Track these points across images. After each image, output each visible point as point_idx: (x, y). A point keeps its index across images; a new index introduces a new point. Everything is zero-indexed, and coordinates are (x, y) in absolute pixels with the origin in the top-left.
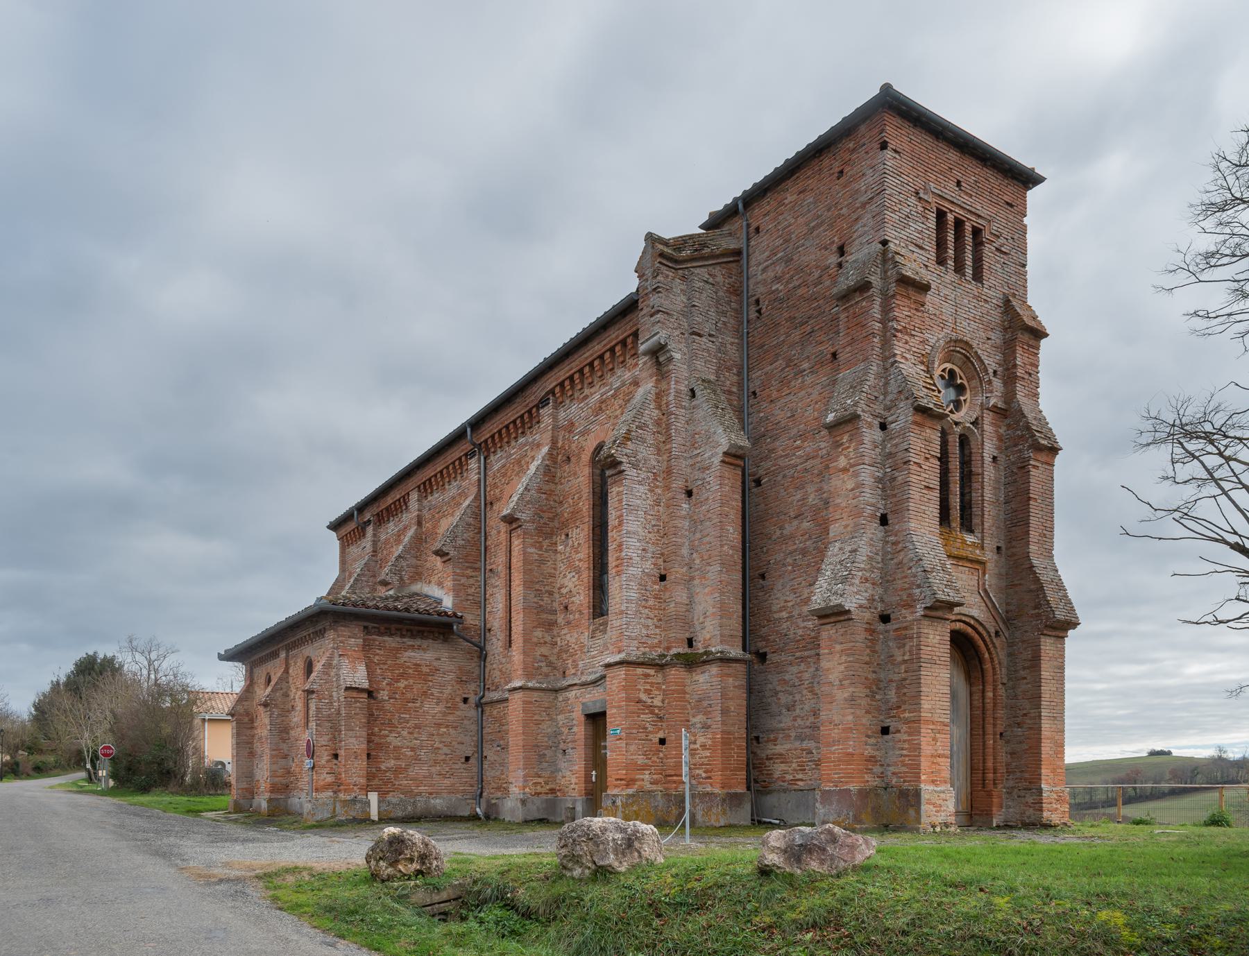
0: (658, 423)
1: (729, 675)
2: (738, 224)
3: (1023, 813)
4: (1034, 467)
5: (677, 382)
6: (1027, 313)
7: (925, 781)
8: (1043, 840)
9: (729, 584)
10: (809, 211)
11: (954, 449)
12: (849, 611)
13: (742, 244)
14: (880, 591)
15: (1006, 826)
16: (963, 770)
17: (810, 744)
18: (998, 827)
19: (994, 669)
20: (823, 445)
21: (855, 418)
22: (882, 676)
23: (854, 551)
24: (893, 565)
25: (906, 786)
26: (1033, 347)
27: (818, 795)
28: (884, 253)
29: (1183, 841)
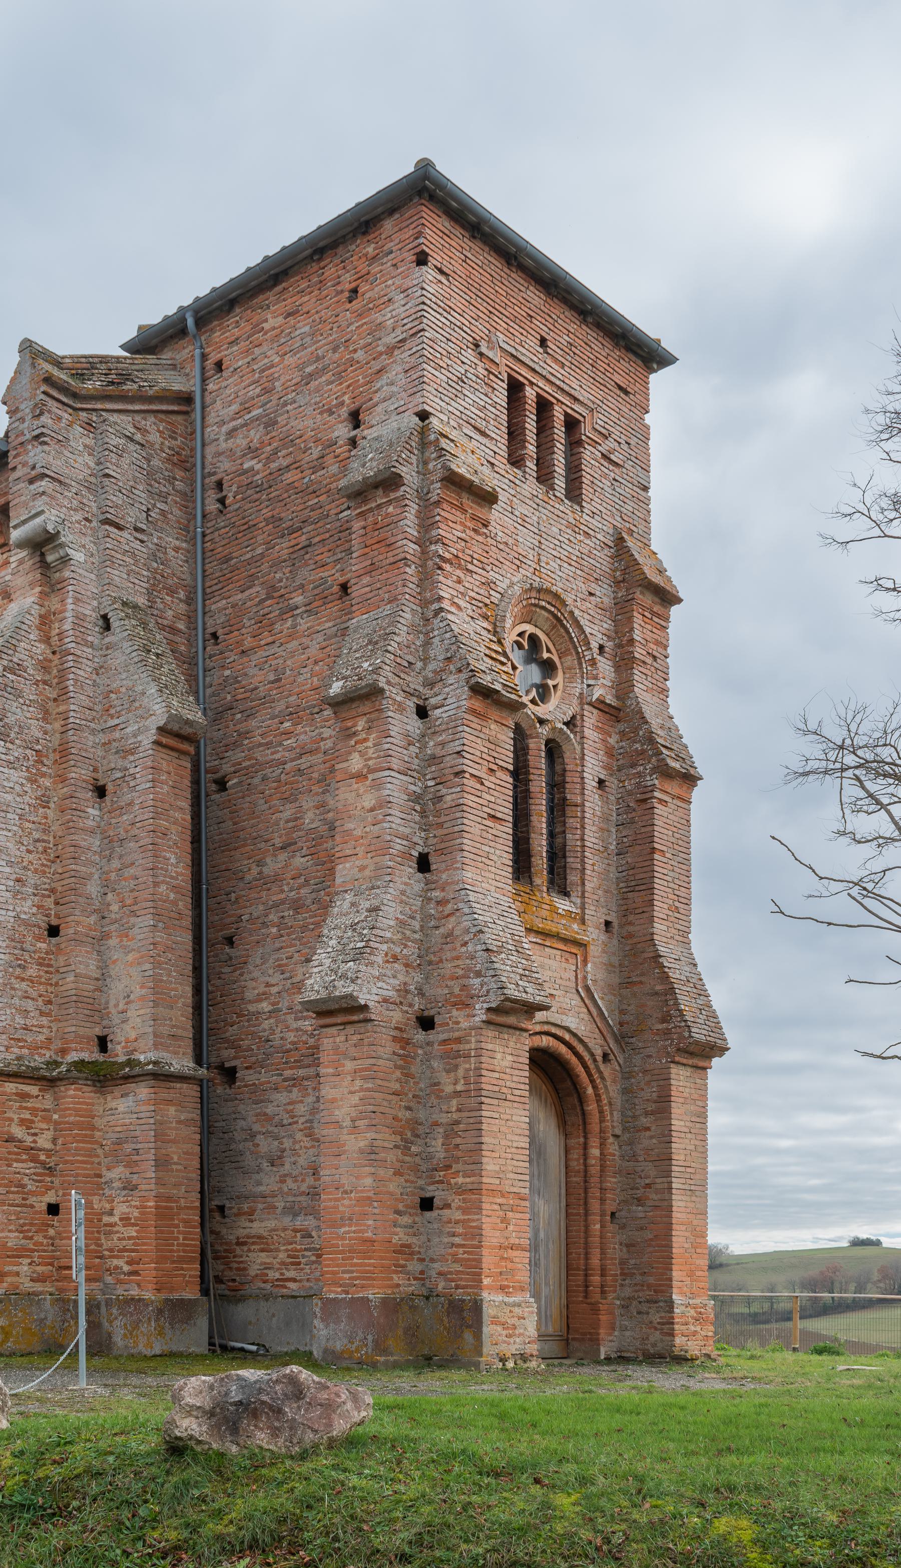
0: (44, 666)
1: (169, 1102)
2: (185, 352)
3: (644, 1339)
4: (661, 801)
5: (77, 601)
6: (649, 562)
7: (489, 1287)
8: (667, 1383)
9: (168, 949)
10: (303, 347)
11: (538, 762)
12: (365, 1008)
13: (192, 385)
14: (418, 977)
15: (621, 1359)
16: (552, 1266)
17: (309, 1222)
18: (608, 1360)
19: (601, 1112)
20: (327, 732)
21: (374, 693)
22: (422, 1115)
23: (375, 909)
24: (437, 935)
25: (459, 1294)
26: (659, 616)
27: (317, 1306)
28: (423, 432)
29: (870, 1387)
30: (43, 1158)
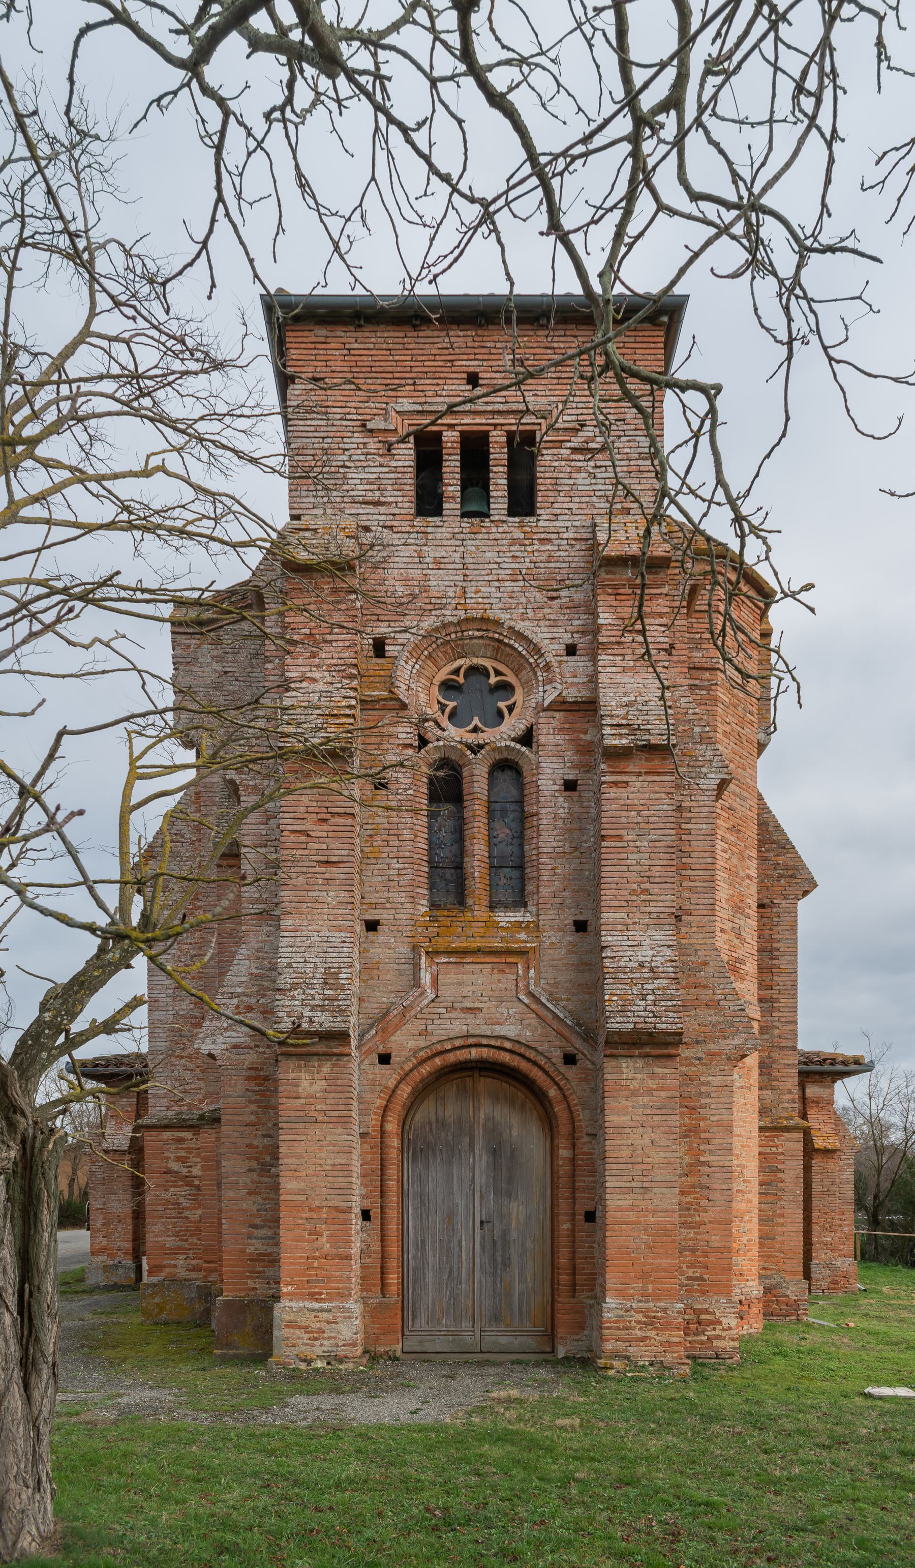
7: (292, 1296)
30: (197, 1182)
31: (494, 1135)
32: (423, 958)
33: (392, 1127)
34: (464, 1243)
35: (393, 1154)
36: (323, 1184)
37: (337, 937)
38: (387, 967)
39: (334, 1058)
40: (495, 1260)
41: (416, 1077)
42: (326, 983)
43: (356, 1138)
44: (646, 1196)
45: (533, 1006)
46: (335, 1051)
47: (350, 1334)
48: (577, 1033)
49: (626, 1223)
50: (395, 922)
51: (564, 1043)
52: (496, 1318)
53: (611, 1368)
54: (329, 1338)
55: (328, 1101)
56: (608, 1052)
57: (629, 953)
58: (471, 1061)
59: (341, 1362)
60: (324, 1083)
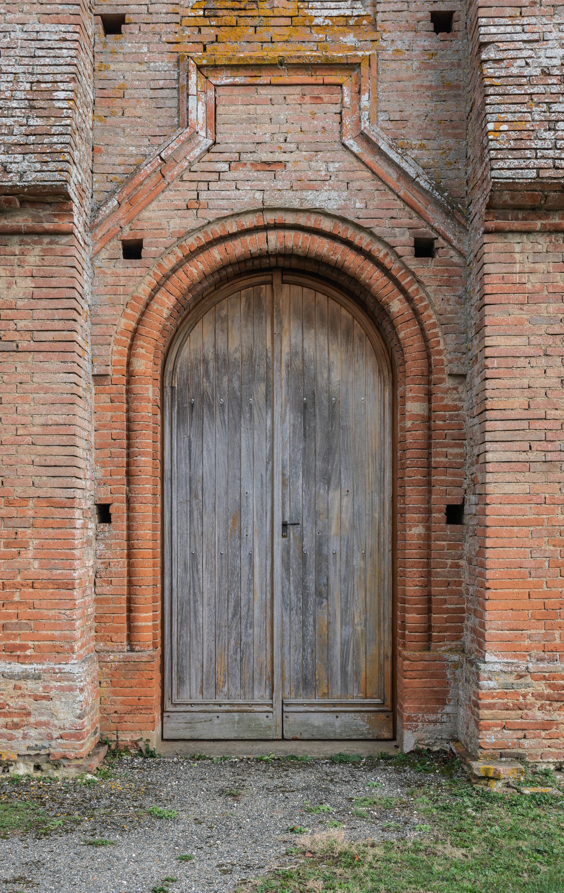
31: (303, 375)
32: (194, 77)
33: (145, 364)
34: (257, 560)
35: (146, 411)
36: (27, 459)
37: (52, 32)
38: (137, 94)
39: (46, 240)
40: (305, 588)
41: (181, 281)
42: (33, 108)
43: (85, 383)
44: (552, 477)
45: (368, 158)
46: (47, 226)
47: (71, 718)
48: (437, 202)
49: (518, 524)
50: (149, 19)
51: (415, 221)
52: (307, 683)
53: (497, 778)
54: (38, 724)
55: (38, 314)
56: (491, 225)
57: (526, 53)
58: (268, 255)
59: (57, 766)
60: (29, 282)
